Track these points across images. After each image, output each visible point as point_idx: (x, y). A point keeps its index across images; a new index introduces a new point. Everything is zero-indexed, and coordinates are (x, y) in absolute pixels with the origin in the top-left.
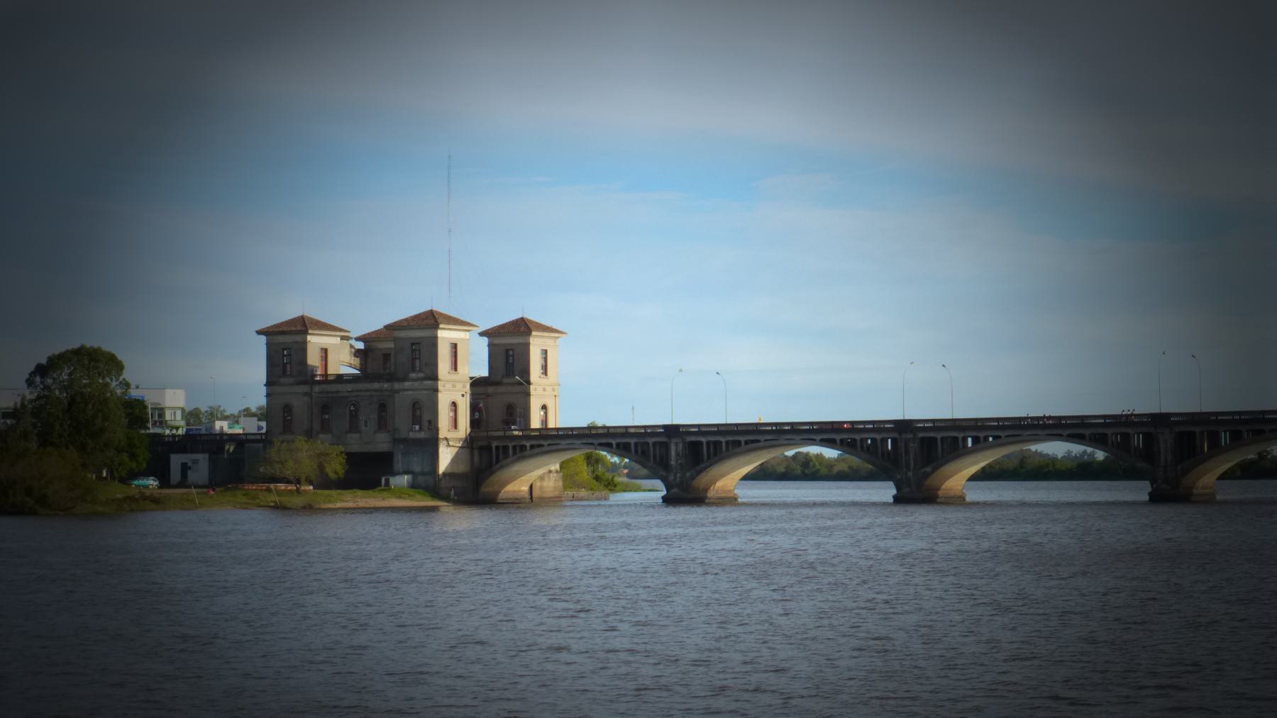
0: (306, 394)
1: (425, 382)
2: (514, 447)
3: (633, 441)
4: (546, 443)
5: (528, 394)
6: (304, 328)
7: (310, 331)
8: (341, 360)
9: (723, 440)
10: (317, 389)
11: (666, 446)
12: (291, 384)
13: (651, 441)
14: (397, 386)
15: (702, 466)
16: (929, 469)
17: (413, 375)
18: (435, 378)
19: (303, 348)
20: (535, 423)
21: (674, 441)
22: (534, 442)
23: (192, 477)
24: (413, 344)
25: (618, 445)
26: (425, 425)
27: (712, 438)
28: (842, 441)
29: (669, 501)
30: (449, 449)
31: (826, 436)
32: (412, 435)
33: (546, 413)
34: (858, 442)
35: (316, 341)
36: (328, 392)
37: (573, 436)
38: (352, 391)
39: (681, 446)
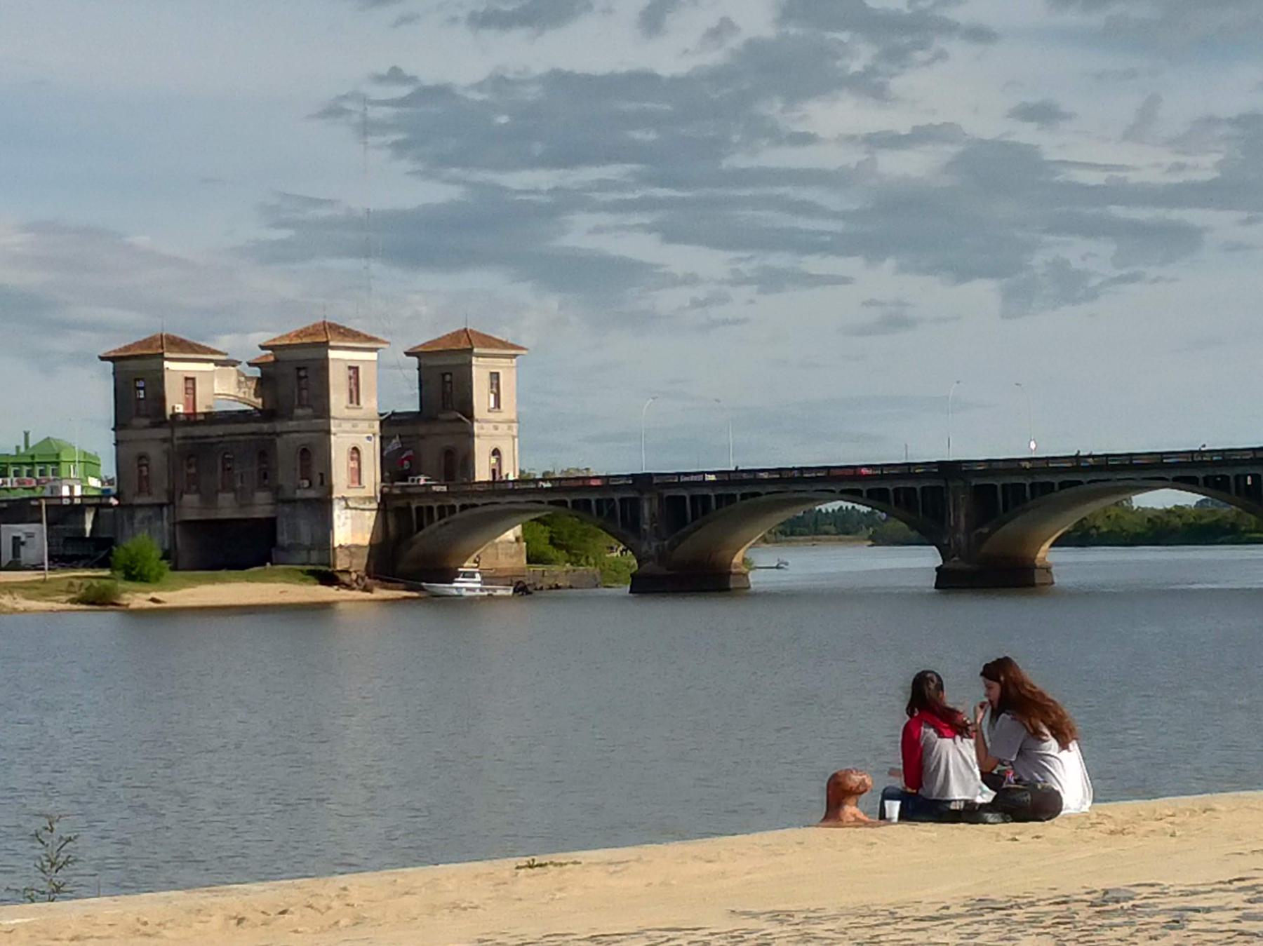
0: (164, 440)
1: (314, 421)
2: (441, 508)
3: (593, 497)
4: (479, 502)
5: (471, 435)
6: (469, 347)
7: (475, 350)
8: (216, 392)
9: (1028, 482)
10: (179, 432)
11: (635, 504)
12: (146, 427)
13: (617, 496)
14: (279, 426)
15: (685, 530)
16: (985, 530)
17: (299, 412)
18: (323, 412)
19: (158, 379)
20: (482, 473)
21: (646, 496)
22: (746, 490)
23: (27, 555)
24: (299, 369)
25: (1205, 479)
26: (317, 480)
27: (901, 484)
28: (869, 492)
29: (644, 585)
30: (348, 511)
31: (1178, 474)
32: (299, 494)
33: (499, 460)
34: (1232, 480)
35: (175, 369)
36: (192, 438)
37: (1114, 469)
38: (223, 436)
39: (656, 502)
